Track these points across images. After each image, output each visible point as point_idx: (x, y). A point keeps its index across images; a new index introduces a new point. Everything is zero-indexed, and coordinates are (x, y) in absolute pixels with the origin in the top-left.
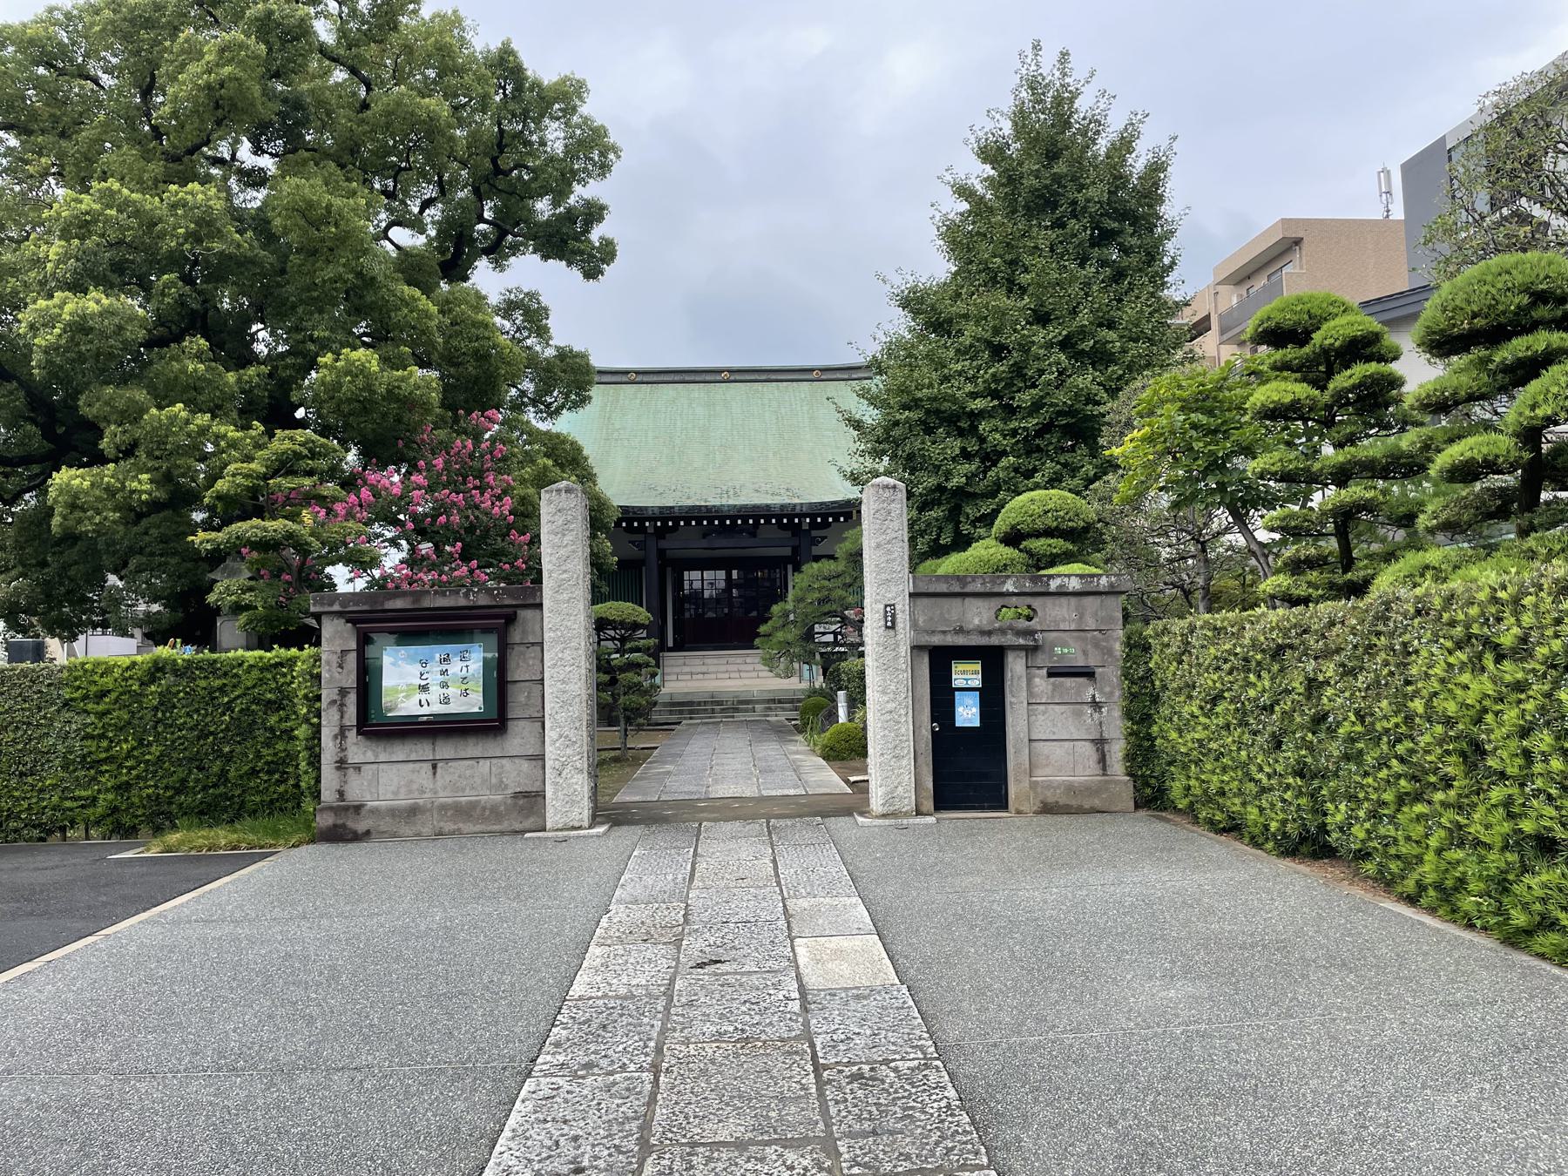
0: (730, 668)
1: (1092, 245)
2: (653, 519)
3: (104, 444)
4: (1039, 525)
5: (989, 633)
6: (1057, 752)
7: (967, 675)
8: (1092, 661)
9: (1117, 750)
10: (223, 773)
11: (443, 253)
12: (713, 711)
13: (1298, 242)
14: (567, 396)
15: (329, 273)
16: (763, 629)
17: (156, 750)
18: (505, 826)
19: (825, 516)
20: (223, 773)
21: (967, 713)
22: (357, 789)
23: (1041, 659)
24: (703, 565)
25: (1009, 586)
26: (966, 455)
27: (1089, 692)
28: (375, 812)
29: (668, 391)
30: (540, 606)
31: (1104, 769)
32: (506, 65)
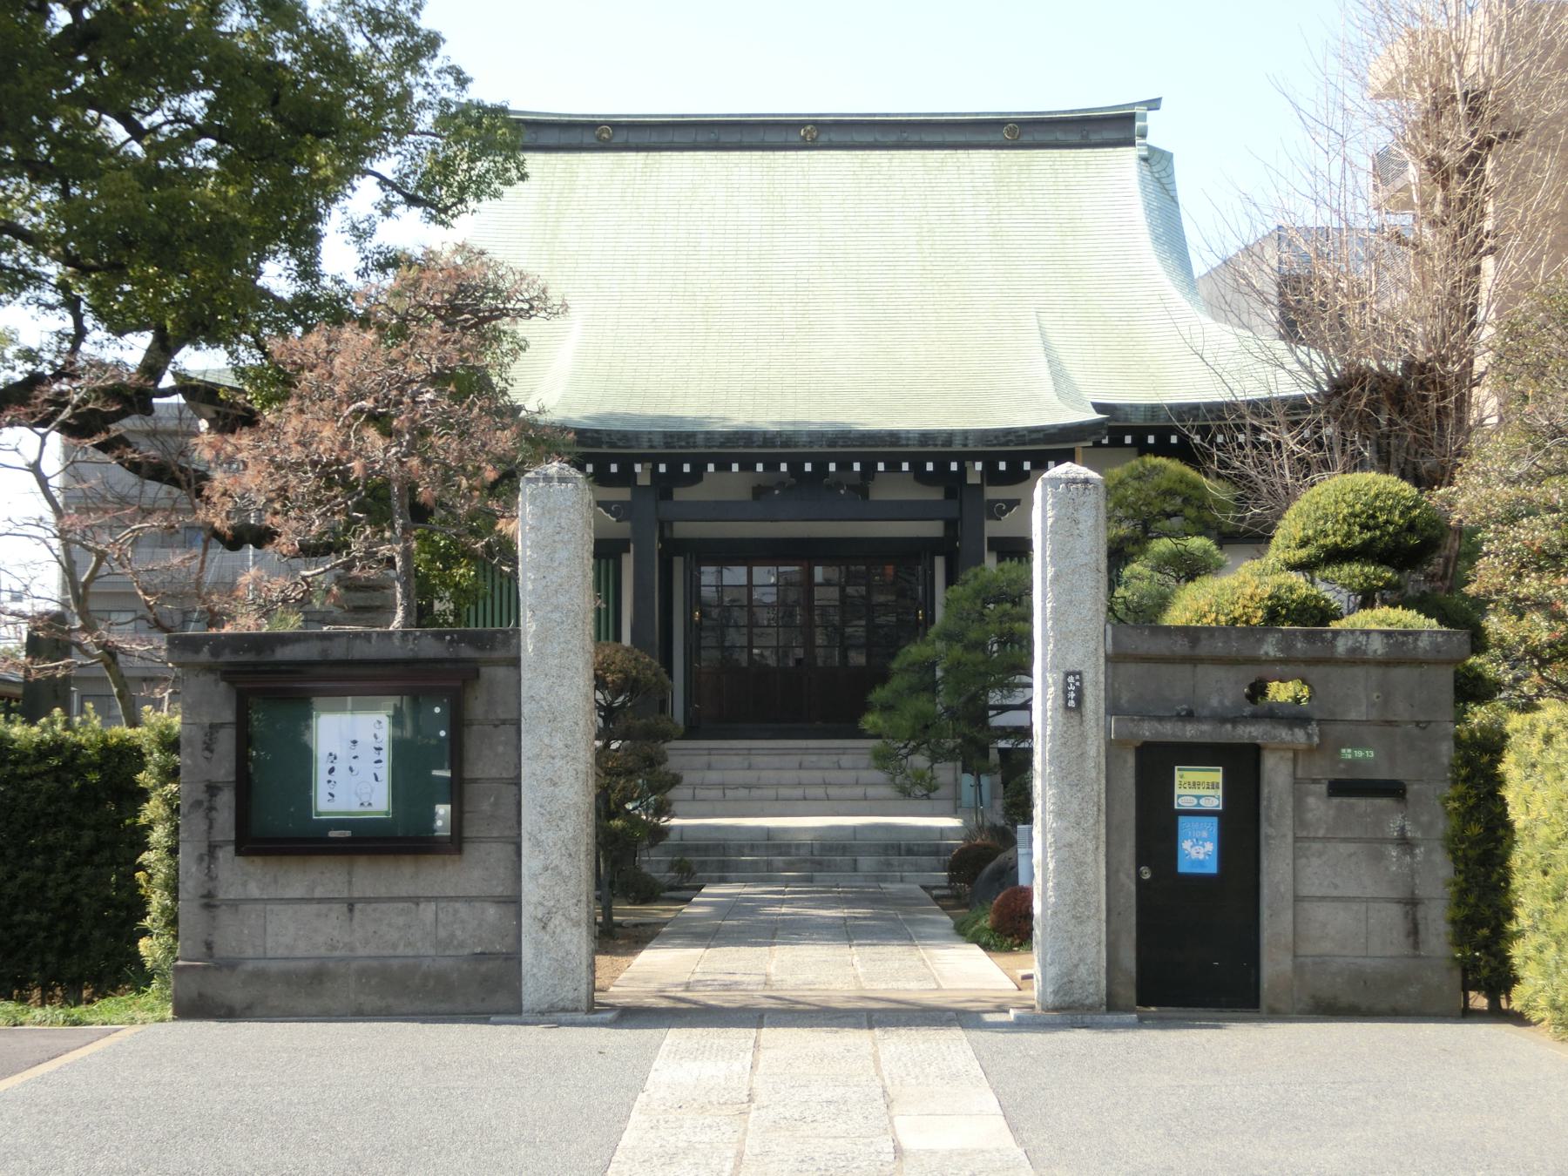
0: (805, 775)
7: (1198, 788)
8: (1399, 774)
12: (769, 866)
16: (879, 694)
19: (1015, 460)
21: (1198, 850)
27: (1394, 824)
30: (515, 662)
31: (1416, 945)
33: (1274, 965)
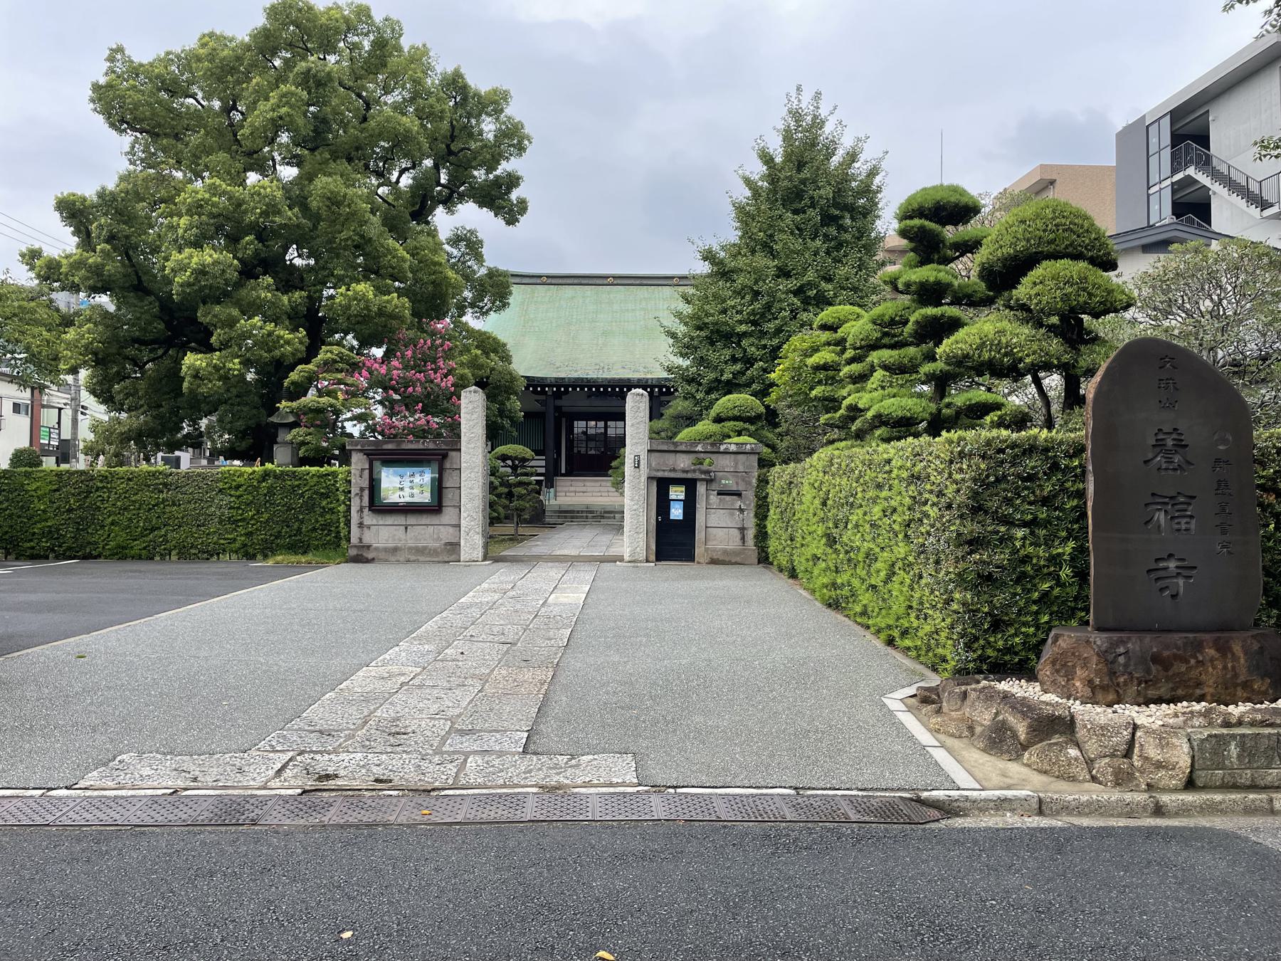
1: (822, 226)
2: (550, 386)
3: (213, 340)
4: (730, 414)
5: (687, 472)
6: (720, 533)
7: (677, 493)
9: (751, 533)
10: (299, 529)
11: (413, 205)
13: (1052, 182)
14: (493, 303)
15: (344, 235)
16: (614, 464)
17: (266, 516)
18: (440, 559)
20: (299, 529)
21: (677, 512)
22: (368, 538)
23: (714, 486)
24: (587, 417)
25: (699, 448)
26: (734, 360)
27: (738, 504)
28: (376, 549)
29: (568, 291)
30: (459, 450)
32: (455, 83)
33: (699, 550)
